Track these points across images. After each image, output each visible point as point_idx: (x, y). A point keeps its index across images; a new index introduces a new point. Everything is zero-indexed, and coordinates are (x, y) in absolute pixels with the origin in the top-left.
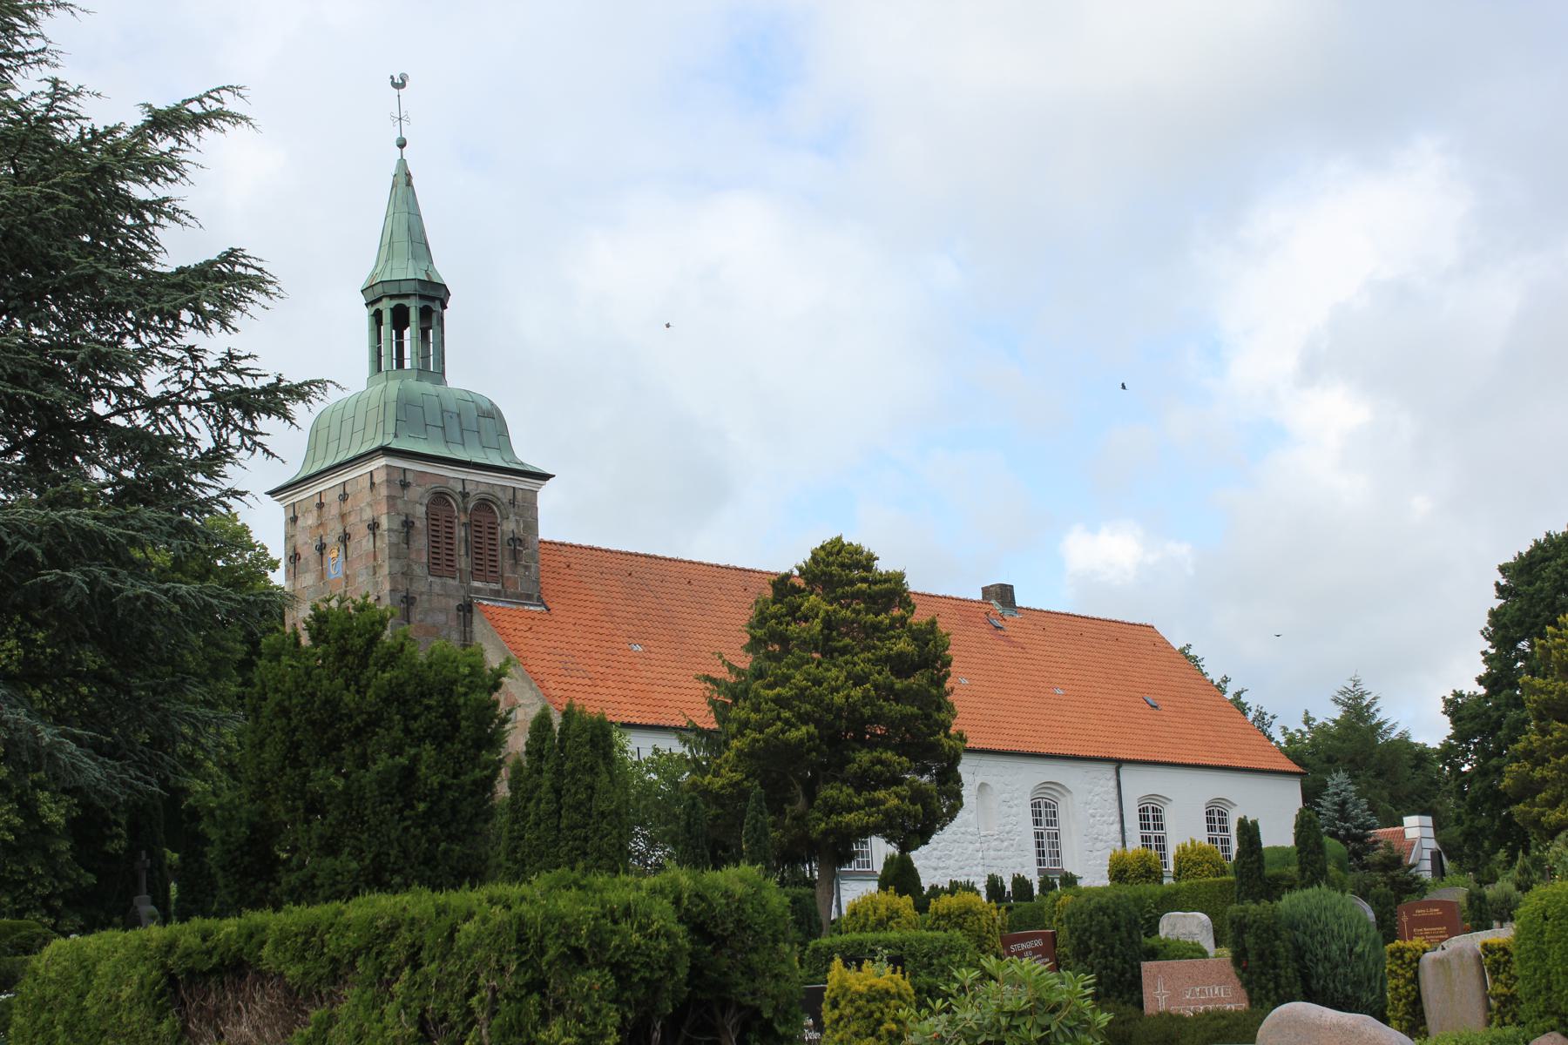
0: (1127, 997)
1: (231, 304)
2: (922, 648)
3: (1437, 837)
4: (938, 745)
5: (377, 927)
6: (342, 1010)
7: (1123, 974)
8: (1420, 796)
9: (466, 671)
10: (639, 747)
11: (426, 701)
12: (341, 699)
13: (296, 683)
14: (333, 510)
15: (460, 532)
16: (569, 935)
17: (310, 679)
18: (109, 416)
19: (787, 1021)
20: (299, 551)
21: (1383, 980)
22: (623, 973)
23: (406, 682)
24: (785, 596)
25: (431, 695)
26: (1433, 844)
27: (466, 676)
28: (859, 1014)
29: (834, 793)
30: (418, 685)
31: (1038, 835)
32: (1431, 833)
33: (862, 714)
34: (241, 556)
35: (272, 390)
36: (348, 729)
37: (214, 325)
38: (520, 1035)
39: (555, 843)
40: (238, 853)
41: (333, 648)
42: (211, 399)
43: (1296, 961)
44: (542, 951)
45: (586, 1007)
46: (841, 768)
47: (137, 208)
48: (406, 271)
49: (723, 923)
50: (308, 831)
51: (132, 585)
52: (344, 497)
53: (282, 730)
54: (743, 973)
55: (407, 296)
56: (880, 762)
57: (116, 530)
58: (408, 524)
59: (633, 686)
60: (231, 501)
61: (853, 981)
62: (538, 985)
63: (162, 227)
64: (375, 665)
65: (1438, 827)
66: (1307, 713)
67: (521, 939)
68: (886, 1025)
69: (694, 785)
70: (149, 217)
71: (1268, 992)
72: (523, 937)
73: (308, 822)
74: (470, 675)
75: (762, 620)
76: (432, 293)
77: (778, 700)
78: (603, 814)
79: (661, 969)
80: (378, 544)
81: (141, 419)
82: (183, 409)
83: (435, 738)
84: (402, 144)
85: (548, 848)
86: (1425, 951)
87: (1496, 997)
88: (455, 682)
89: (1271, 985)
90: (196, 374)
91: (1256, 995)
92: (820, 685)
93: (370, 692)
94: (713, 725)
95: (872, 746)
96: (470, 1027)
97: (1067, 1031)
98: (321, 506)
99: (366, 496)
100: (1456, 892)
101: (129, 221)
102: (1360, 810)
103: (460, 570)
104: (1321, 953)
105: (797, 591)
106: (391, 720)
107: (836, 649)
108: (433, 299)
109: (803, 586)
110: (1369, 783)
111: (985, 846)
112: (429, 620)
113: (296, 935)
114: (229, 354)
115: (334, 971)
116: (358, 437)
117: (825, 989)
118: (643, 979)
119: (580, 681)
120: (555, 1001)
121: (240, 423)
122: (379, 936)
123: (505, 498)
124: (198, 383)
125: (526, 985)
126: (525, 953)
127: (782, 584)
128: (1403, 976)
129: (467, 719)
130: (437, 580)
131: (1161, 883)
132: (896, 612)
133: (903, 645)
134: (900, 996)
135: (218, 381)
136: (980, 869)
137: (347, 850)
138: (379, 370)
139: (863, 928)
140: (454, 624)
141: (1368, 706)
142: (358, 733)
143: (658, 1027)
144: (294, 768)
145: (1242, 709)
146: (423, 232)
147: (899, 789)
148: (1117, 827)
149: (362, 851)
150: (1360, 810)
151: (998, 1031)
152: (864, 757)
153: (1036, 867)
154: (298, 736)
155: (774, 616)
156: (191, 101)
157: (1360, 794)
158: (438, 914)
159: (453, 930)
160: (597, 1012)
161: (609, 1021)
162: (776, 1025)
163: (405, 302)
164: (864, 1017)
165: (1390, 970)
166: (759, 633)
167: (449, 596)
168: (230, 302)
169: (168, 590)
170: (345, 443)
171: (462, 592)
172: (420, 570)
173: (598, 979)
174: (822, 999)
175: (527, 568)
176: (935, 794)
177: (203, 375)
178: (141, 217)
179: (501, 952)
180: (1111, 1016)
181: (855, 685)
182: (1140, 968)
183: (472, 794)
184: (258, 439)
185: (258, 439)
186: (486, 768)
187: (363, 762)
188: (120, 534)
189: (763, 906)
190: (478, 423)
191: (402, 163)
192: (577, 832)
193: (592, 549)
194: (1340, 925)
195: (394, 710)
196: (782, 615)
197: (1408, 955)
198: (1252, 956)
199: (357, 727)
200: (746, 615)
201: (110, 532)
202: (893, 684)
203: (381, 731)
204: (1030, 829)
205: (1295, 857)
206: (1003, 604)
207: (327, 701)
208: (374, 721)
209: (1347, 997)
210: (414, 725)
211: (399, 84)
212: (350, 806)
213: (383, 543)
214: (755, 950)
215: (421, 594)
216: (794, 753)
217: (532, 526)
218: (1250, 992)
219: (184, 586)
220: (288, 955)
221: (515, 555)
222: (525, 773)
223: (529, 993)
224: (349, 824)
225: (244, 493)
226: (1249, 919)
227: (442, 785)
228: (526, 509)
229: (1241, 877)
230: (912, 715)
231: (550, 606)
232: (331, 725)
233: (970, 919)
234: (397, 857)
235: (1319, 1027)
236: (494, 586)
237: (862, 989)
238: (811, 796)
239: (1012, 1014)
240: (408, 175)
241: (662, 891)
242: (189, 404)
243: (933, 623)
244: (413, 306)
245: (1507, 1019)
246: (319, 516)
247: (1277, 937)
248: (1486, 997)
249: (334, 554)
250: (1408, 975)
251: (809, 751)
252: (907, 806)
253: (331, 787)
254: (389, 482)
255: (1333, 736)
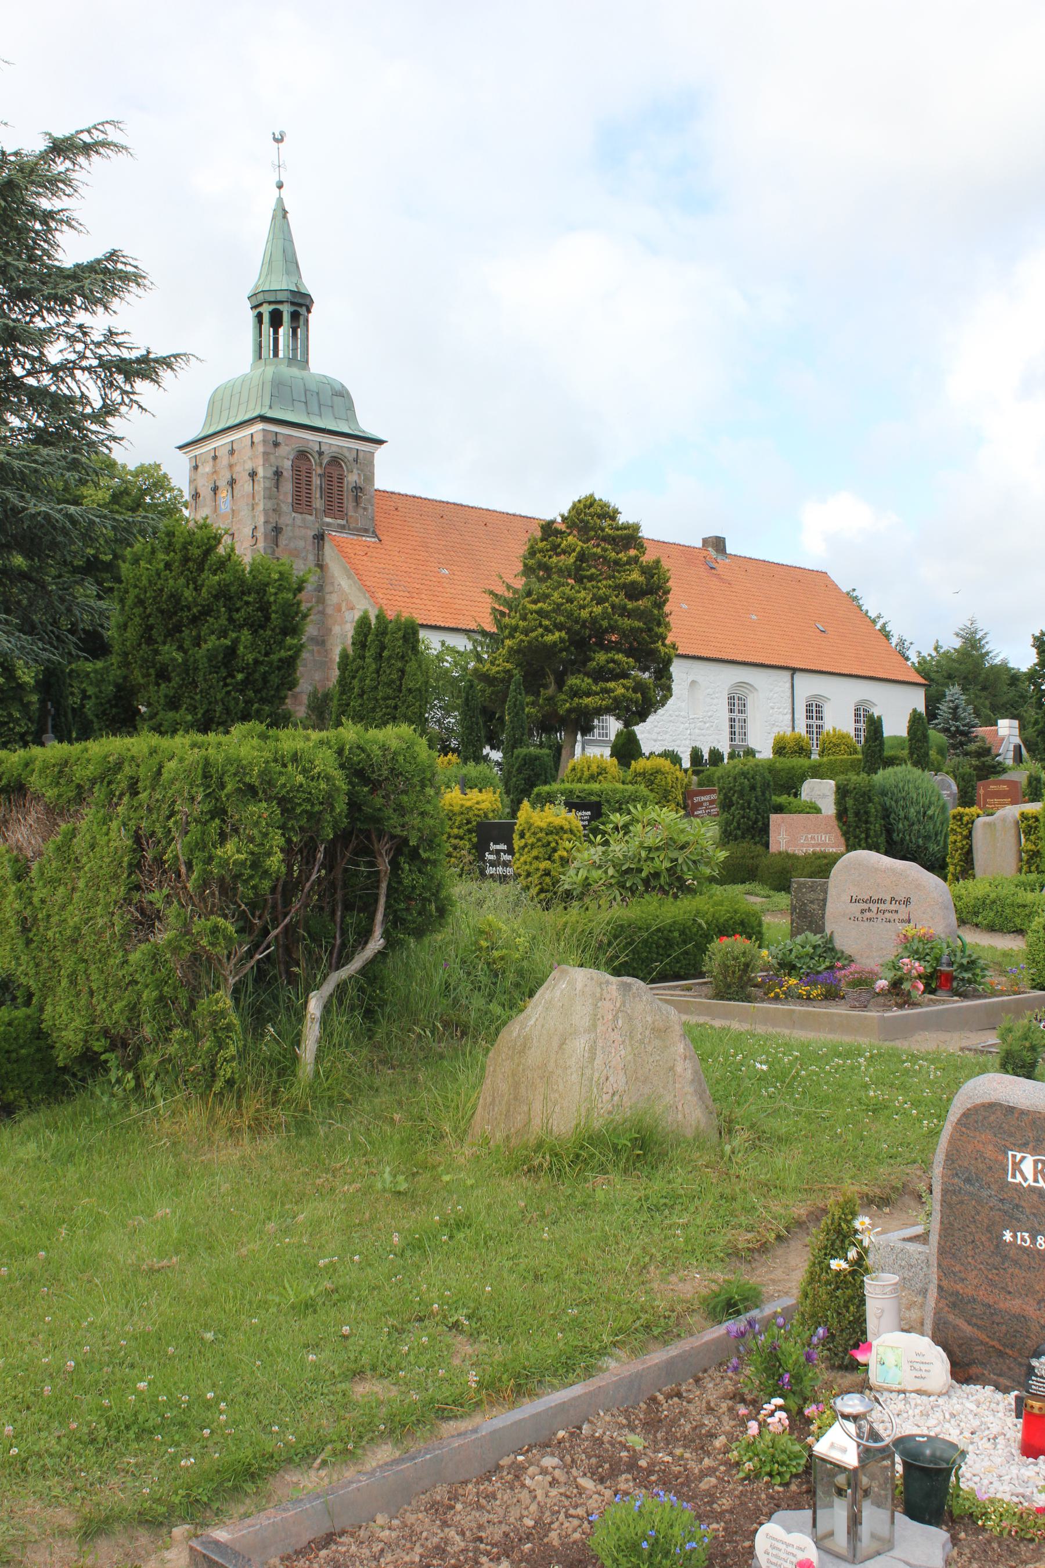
0: (757, 839)
1: (113, 292)
2: (648, 580)
3: (1020, 735)
4: (657, 651)
5: (109, 762)
6: (83, 825)
7: (756, 822)
8: (1012, 706)
9: (276, 576)
10: (432, 642)
11: (245, 598)
12: (182, 595)
13: (150, 581)
14: (224, 460)
15: (316, 481)
16: (245, 774)
17: (159, 578)
18: (22, 377)
19: (431, 848)
20: (199, 491)
21: (946, 836)
22: (289, 806)
23: (231, 584)
24: (550, 536)
25: (250, 593)
26: (1017, 740)
27: (276, 581)
28: (540, 844)
29: (578, 682)
30: (240, 586)
31: (732, 720)
32: (1016, 732)
33: (601, 626)
34: (163, 495)
35: (144, 360)
36: (187, 616)
37: (100, 309)
38: (203, 851)
39: (373, 710)
40: (108, 706)
41: (178, 557)
42: (99, 366)
43: (884, 819)
44: (222, 786)
45: (255, 832)
46: (584, 663)
47: (47, 217)
48: (281, 283)
49: (379, 770)
50: (157, 692)
51: (35, 505)
52: (232, 452)
53: (140, 615)
54: (395, 810)
55: (281, 302)
56: (613, 661)
57: (22, 463)
58: (278, 474)
59: (440, 599)
60: (112, 445)
61: (537, 819)
62: (219, 812)
63: (61, 232)
64: (209, 570)
65: (1022, 728)
66: (937, 642)
67: (206, 776)
68: (559, 853)
69: (476, 670)
70: (53, 225)
71: (860, 841)
72: (208, 774)
73: (158, 685)
74: (279, 580)
75: (532, 553)
76: (300, 301)
77: (540, 613)
78: (410, 691)
79: (322, 803)
80: (256, 487)
81: (46, 379)
82: (78, 373)
83: (252, 626)
84: (280, 186)
85: (368, 712)
86: (978, 816)
87: (1027, 852)
88: (267, 585)
89: (863, 836)
90: (86, 346)
91: (851, 842)
92: (572, 603)
93: (204, 590)
94: (494, 630)
95: (607, 649)
96: (169, 843)
97: (690, 863)
98: (215, 458)
99: (248, 452)
100: (1020, 776)
101: (38, 226)
102: (967, 714)
103: (316, 509)
104: (902, 814)
105: (558, 533)
106: (219, 611)
107: (585, 577)
108: (300, 305)
109: (564, 529)
110: (975, 694)
111: (692, 726)
112: (292, 545)
113: (54, 766)
114: (110, 331)
115: (79, 794)
116: (243, 407)
117: (515, 824)
118: (306, 811)
119: (401, 594)
120: (233, 826)
121: (122, 385)
122: (109, 769)
123: (351, 457)
124: (88, 353)
125: (210, 812)
126: (209, 787)
127: (548, 529)
128: (961, 833)
129: (276, 612)
130: (298, 516)
131: (810, 758)
132: (633, 552)
133: (635, 576)
134: (572, 832)
135: (101, 351)
136: (688, 742)
137: (185, 706)
138: (260, 358)
139: (579, 780)
140: (310, 548)
141: (980, 640)
142: (194, 620)
143: (322, 849)
144: (148, 644)
145: (887, 636)
146: (294, 254)
147: (625, 681)
148: (789, 717)
149: (195, 708)
150: (967, 714)
151: (639, 860)
152: (601, 657)
153: (728, 743)
154: (151, 621)
155: (541, 551)
156: (82, 131)
157: (968, 702)
158: (151, 754)
159: (161, 767)
160: (265, 835)
161: (275, 843)
162: (421, 851)
163: (280, 307)
164: (543, 846)
165: (952, 829)
166: (531, 562)
167: (307, 528)
168: (113, 292)
169: (62, 509)
170: (233, 412)
171: (317, 525)
172: (286, 508)
173: (266, 809)
174: (513, 831)
175: (365, 509)
176: (652, 686)
177: (92, 347)
178: (47, 224)
179: (191, 786)
180: (727, 854)
181: (597, 604)
182: (768, 818)
183: (279, 668)
184: (134, 397)
185: (134, 397)
186: (290, 649)
187: (197, 642)
188: (25, 466)
189: (415, 758)
190: (332, 401)
191: (280, 201)
192: (390, 702)
193: (414, 497)
194: (918, 794)
195: (221, 603)
196: (548, 551)
197: (965, 819)
198: (850, 814)
199: (194, 616)
200: (523, 550)
201: (16, 464)
202: (626, 605)
203: (211, 620)
204: (726, 715)
205: (907, 744)
206: (717, 551)
207: (172, 596)
208: (207, 611)
209: (918, 847)
210: (236, 616)
211: (279, 140)
212: (188, 674)
213: (260, 487)
214: (405, 792)
215: (287, 525)
216: (550, 651)
217: (370, 478)
218: (847, 840)
219: (72, 507)
220: (48, 781)
221: (357, 500)
222: (351, 658)
223: (213, 818)
224: (187, 687)
225: (122, 439)
226: (851, 787)
227: (256, 662)
228: (366, 466)
229: (866, 757)
230: (639, 628)
231: (381, 537)
232: (175, 613)
233: (659, 777)
234: (221, 713)
235: (877, 869)
236: (343, 522)
237: (543, 825)
238: (560, 684)
239: (650, 849)
240: (285, 212)
241: (328, 743)
242: (83, 369)
243: (658, 562)
244: (286, 310)
245: (1033, 868)
246: (214, 466)
247: (870, 800)
248: (1020, 852)
249: (224, 494)
250: (964, 833)
251: (561, 650)
252: (630, 694)
253: (173, 659)
254: (265, 442)
255: (954, 660)
